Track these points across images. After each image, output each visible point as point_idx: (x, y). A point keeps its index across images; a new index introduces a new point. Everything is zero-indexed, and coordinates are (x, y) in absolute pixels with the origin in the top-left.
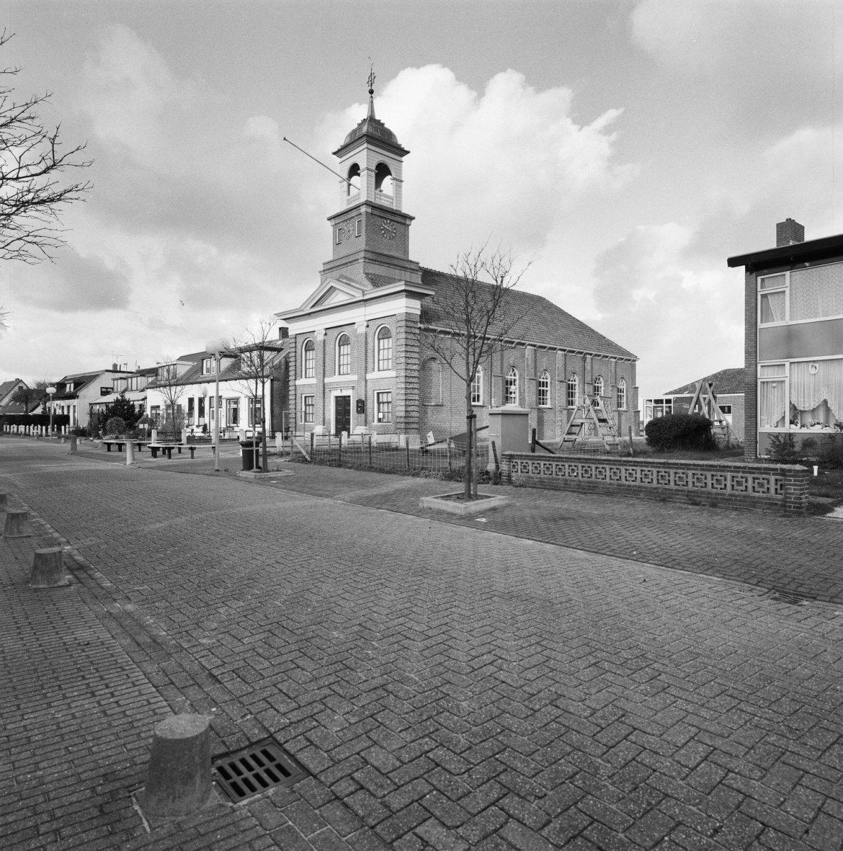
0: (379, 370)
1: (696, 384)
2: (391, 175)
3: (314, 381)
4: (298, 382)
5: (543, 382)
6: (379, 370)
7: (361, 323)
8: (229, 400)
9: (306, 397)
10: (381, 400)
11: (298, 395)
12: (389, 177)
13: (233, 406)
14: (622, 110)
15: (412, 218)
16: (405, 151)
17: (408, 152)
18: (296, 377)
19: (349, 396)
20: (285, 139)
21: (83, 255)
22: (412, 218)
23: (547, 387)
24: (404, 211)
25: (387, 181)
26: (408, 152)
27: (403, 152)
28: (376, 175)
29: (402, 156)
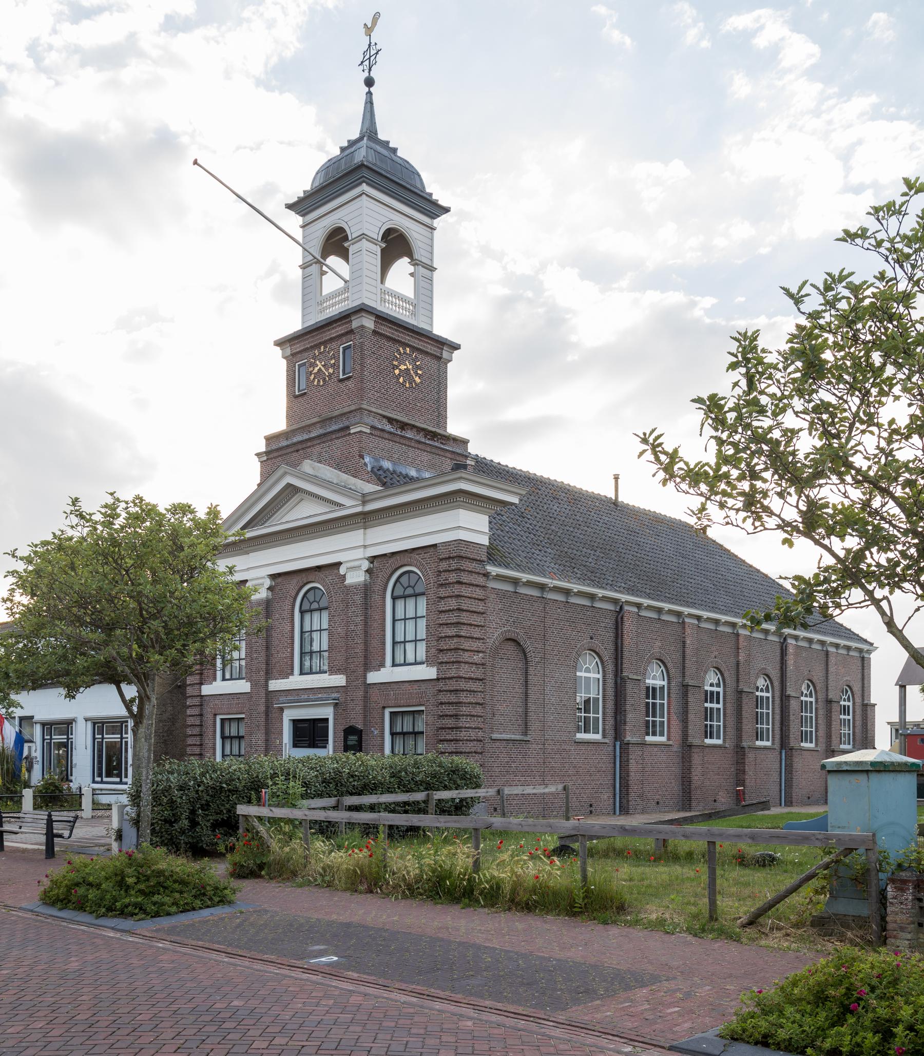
0: (394, 665)
1: (326, 668)
2: (410, 254)
3: (243, 686)
4: (206, 690)
5: (712, 693)
6: (394, 665)
7: (356, 563)
8: (48, 726)
9: (222, 720)
10: (227, 734)
11: (208, 717)
12: (405, 260)
13: (59, 738)
14: (594, 8)
15: (456, 347)
16: (435, 204)
17: (447, 210)
18: (201, 679)
19: (327, 720)
20: (195, 162)
21: (462, 512)
22: (456, 347)
23: (718, 702)
24: (440, 329)
25: (402, 266)
26: (447, 210)
27: (434, 209)
28: (383, 251)
29: (434, 216)
